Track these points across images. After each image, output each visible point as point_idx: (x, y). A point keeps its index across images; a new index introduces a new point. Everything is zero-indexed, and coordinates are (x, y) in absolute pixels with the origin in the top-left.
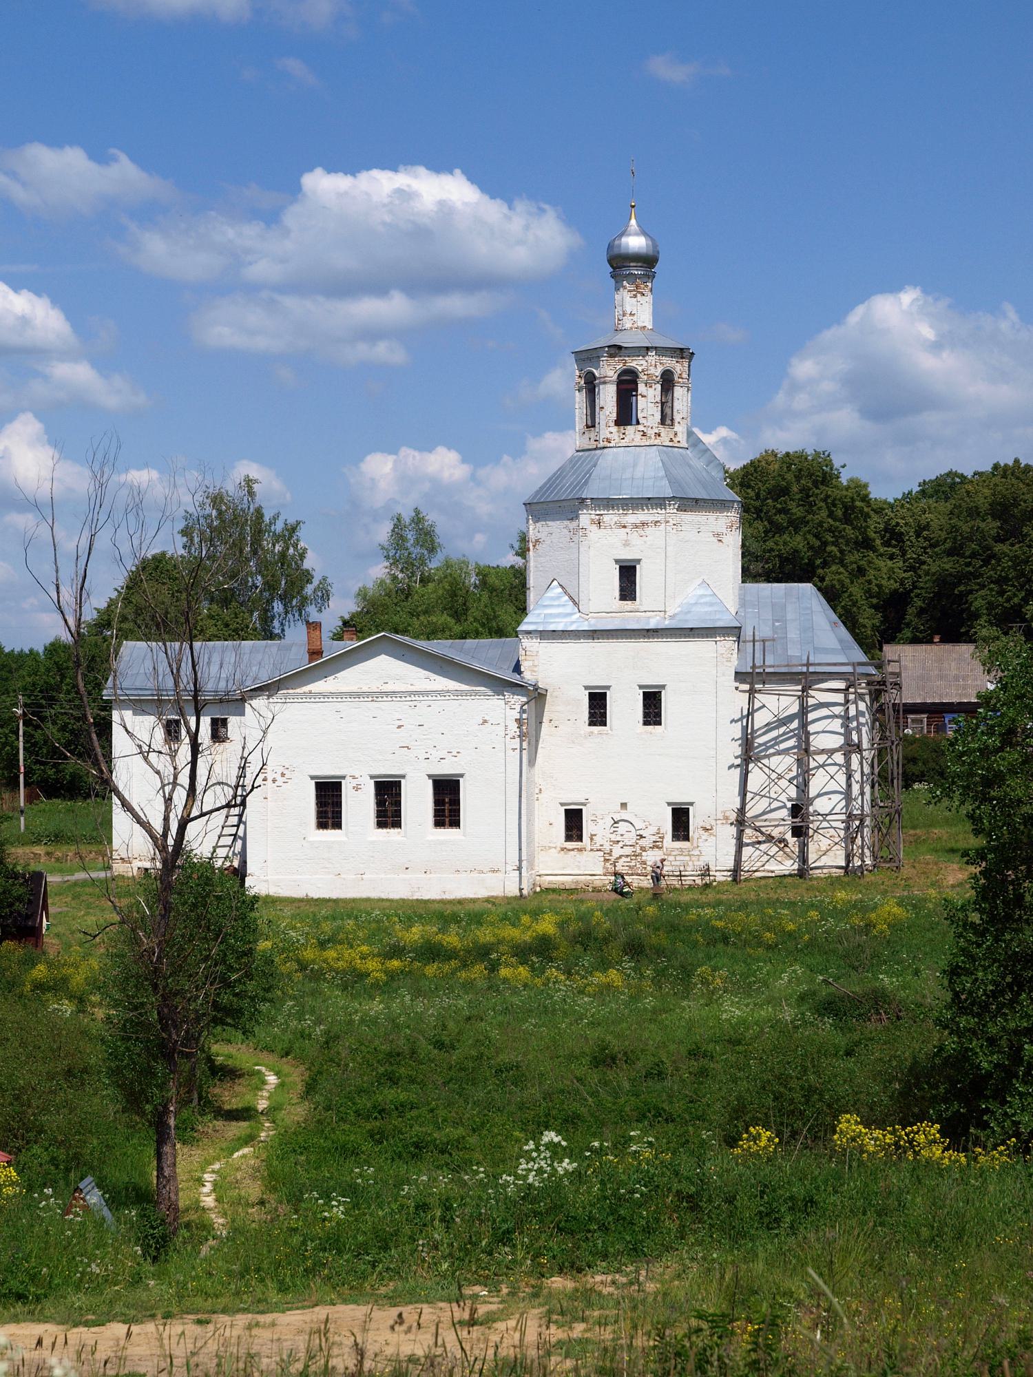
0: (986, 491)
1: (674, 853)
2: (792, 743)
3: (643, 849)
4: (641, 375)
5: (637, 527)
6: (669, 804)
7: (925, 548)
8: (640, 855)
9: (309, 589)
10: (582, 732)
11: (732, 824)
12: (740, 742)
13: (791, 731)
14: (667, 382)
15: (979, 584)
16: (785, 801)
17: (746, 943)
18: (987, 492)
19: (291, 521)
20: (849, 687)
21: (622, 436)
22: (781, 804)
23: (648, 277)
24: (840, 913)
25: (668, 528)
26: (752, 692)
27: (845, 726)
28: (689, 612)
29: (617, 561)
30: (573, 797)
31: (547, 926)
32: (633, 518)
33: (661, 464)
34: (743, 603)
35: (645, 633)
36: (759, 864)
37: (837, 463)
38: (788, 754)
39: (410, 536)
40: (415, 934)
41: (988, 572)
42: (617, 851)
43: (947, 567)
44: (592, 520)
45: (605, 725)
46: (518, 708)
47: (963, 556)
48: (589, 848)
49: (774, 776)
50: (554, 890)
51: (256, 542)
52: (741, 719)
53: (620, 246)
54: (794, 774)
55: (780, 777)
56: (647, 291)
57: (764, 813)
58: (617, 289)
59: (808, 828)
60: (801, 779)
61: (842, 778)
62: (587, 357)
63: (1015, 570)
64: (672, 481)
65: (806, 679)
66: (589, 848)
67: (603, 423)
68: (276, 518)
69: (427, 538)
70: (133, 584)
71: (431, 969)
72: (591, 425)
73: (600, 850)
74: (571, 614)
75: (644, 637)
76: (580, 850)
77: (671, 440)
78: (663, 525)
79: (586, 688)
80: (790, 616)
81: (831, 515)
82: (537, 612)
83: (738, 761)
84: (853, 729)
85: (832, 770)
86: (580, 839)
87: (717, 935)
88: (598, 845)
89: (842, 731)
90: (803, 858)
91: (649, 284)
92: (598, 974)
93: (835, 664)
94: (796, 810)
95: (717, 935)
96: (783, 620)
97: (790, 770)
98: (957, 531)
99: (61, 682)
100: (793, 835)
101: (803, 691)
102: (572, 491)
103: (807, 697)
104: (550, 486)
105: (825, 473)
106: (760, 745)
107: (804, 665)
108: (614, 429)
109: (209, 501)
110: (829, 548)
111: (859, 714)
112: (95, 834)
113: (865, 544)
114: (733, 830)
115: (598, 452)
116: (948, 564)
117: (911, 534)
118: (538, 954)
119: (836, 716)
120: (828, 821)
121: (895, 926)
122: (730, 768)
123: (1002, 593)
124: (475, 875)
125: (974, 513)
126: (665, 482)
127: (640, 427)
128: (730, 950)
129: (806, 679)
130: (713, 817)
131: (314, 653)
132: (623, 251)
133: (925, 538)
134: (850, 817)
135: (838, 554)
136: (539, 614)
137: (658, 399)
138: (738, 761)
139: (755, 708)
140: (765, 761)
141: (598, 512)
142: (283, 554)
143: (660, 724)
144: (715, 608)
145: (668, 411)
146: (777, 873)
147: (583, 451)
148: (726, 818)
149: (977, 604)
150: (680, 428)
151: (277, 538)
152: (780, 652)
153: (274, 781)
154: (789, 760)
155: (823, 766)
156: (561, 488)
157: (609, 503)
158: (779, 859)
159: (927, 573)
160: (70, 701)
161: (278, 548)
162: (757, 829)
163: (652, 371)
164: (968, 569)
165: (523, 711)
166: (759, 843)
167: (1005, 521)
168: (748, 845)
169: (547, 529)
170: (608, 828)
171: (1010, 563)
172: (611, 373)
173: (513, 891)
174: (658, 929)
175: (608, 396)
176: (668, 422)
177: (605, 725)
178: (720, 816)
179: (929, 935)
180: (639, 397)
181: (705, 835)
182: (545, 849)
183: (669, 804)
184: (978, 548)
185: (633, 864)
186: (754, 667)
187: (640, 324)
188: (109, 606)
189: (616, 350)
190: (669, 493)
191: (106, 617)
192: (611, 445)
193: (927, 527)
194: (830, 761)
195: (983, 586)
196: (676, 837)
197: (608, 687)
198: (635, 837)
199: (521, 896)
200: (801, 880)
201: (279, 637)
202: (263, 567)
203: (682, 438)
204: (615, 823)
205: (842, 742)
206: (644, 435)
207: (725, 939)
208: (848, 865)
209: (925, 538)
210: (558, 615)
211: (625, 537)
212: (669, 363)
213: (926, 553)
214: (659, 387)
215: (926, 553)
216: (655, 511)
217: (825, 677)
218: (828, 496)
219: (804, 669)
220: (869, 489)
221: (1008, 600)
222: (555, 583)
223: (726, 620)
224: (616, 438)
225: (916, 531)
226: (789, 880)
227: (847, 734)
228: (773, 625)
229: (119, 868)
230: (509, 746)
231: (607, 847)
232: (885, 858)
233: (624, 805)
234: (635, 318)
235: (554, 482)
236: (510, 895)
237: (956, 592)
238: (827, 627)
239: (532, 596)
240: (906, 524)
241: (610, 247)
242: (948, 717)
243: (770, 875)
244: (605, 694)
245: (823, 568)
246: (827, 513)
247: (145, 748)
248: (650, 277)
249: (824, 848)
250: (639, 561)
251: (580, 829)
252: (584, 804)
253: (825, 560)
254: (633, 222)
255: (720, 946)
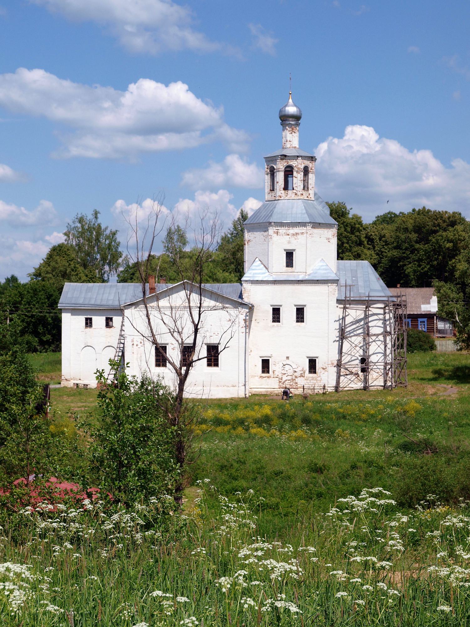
0: (411, 220)
1: (310, 379)
2: (361, 331)
3: (296, 377)
4: (295, 168)
5: (294, 235)
6: (308, 357)
7: (383, 246)
8: (295, 380)
9: (120, 260)
10: (269, 325)
11: (335, 366)
12: (338, 330)
13: (361, 325)
14: (306, 171)
15: (408, 262)
16: (358, 356)
17: (354, 419)
18: (412, 221)
19: (114, 230)
20: (386, 306)
21: (286, 195)
22: (356, 358)
23: (297, 125)
24: (392, 406)
25: (308, 236)
26: (345, 308)
27: (384, 324)
28: (316, 273)
29: (285, 250)
30: (265, 354)
31: (267, 410)
32: (292, 231)
33: (304, 208)
34: (338, 269)
35: (297, 282)
36: (347, 384)
37: (348, 208)
38: (360, 336)
39: (175, 237)
40: (210, 413)
41: (413, 256)
42: (285, 378)
43: (395, 254)
44: (274, 232)
45: (279, 322)
46: (244, 314)
47: (401, 249)
48: (272, 376)
49: (354, 345)
50: (257, 395)
51: (97, 239)
52: (339, 320)
53: (285, 111)
54: (362, 345)
55: (356, 346)
56: (296, 131)
57: (349, 362)
58: (283, 130)
59: (368, 368)
60: (365, 347)
61: (382, 347)
62: (271, 160)
63: (426, 256)
64: (309, 215)
65: (368, 303)
66: (272, 376)
67: (278, 189)
68: (106, 228)
69: (183, 239)
70: (50, 256)
71: (219, 429)
72: (273, 189)
73: (277, 377)
74: (265, 273)
75: (297, 283)
76: (268, 377)
77: (308, 197)
78: (305, 234)
79: (271, 306)
80: (359, 275)
81: (345, 230)
82: (250, 272)
83: (338, 339)
84: (388, 325)
85: (379, 343)
86: (268, 372)
87: (341, 415)
88: (276, 375)
89: (382, 326)
90: (366, 380)
91: (297, 128)
92: (293, 432)
93: (380, 297)
94: (363, 361)
95: (341, 415)
96: (356, 277)
97: (360, 343)
98: (399, 238)
99: (22, 300)
100: (362, 372)
101: (366, 308)
102: (265, 219)
103: (368, 311)
104: (255, 217)
105: (343, 212)
106: (347, 332)
107: (367, 297)
108: (283, 192)
109: (77, 220)
110: (345, 245)
111: (390, 319)
112: (41, 368)
113: (360, 244)
114: (335, 369)
115: (276, 202)
116: (395, 253)
117: (377, 239)
118: (266, 423)
119: (380, 319)
120: (376, 366)
121: (418, 412)
122: (334, 342)
123: (419, 266)
124: (225, 388)
125: (406, 230)
126: (306, 215)
127: (294, 191)
128: (347, 422)
129: (368, 303)
130: (327, 363)
131: (152, 289)
132: (286, 113)
133: (383, 241)
134: (386, 364)
135: (349, 248)
136: (251, 273)
137: (302, 179)
138: (338, 339)
139: (346, 315)
140: (349, 339)
141: (277, 228)
142: (110, 245)
143: (303, 322)
144: (328, 271)
145: (306, 184)
146: (355, 388)
147: (269, 201)
148: (333, 364)
149: (409, 270)
150: (311, 192)
151: (107, 237)
152: (355, 291)
153: (137, 345)
154: (360, 339)
155: (374, 341)
156: (260, 217)
157: (282, 224)
158: (355, 382)
159: (386, 257)
160: (25, 309)
161: (107, 242)
162: (346, 369)
163: (300, 166)
164: (403, 255)
165: (246, 316)
166: (347, 375)
167: (420, 234)
168: (342, 376)
169: (253, 235)
170: (281, 367)
171: (423, 253)
172: (282, 167)
173: (242, 395)
174: (314, 413)
175: (280, 177)
176: (306, 189)
177: (279, 322)
178: (330, 363)
179: (432, 416)
180: (294, 178)
181: (323, 371)
182: (253, 376)
183: (308, 357)
184: (408, 246)
185: (291, 383)
186: (346, 297)
187: (294, 146)
188: (40, 267)
189: (284, 157)
190: (308, 220)
191: (38, 272)
192: (282, 199)
193: (384, 236)
194: (377, 339)
195: (410, 263)
196: (310, 372)
197: (281, 306)
198: (293, 372)
199: (246, 397)
200: (366, 392)
201: (107, 281)
202: (100, 250)
203: (312, 196)
204: (284, 365)
205: (383, 331)
206: (296, 194)
207: (344, 417)
208: (385, 385)
209: (383, 241)
210: (259, 274)
211: (288, 239)
212: (307, 163)
213: (384, 248)
214: (302, 173)
215: (384, 248)
216: (302, 228)
217: (374, 302)
218: (344, 222)
219: (367, 299)
220: (362, 219)
221: (422, 269)
222: (257, 259)
223: (333, 276)
224: (284, 196)
225: (379, 238)
226: (360, 391)
227: (385, 327)
228: (352, 279)
229: (64, 383)
230: (240, 331)
231: (280, 376)
232: (399, 383)
233: (288, 358)
234: (291, 143)
235: (256, 214)
236: (241, 397)
237: (399, 265)
238: (375, 280)
239: (246, 265)
240: (375, 235)
241: (281, 111)
242: (420, 320)
243: (351, 389)
244: (279, 309)
245: (342, 254)
246: (344, 229)
247: (172, 330)
248: (298, 125)
249: (375, 377)
250: (294, 250)
251: (268, 368)
252: (270, 357)
253: (343, 250)
254: (290, 100)
255: (342, 420)
